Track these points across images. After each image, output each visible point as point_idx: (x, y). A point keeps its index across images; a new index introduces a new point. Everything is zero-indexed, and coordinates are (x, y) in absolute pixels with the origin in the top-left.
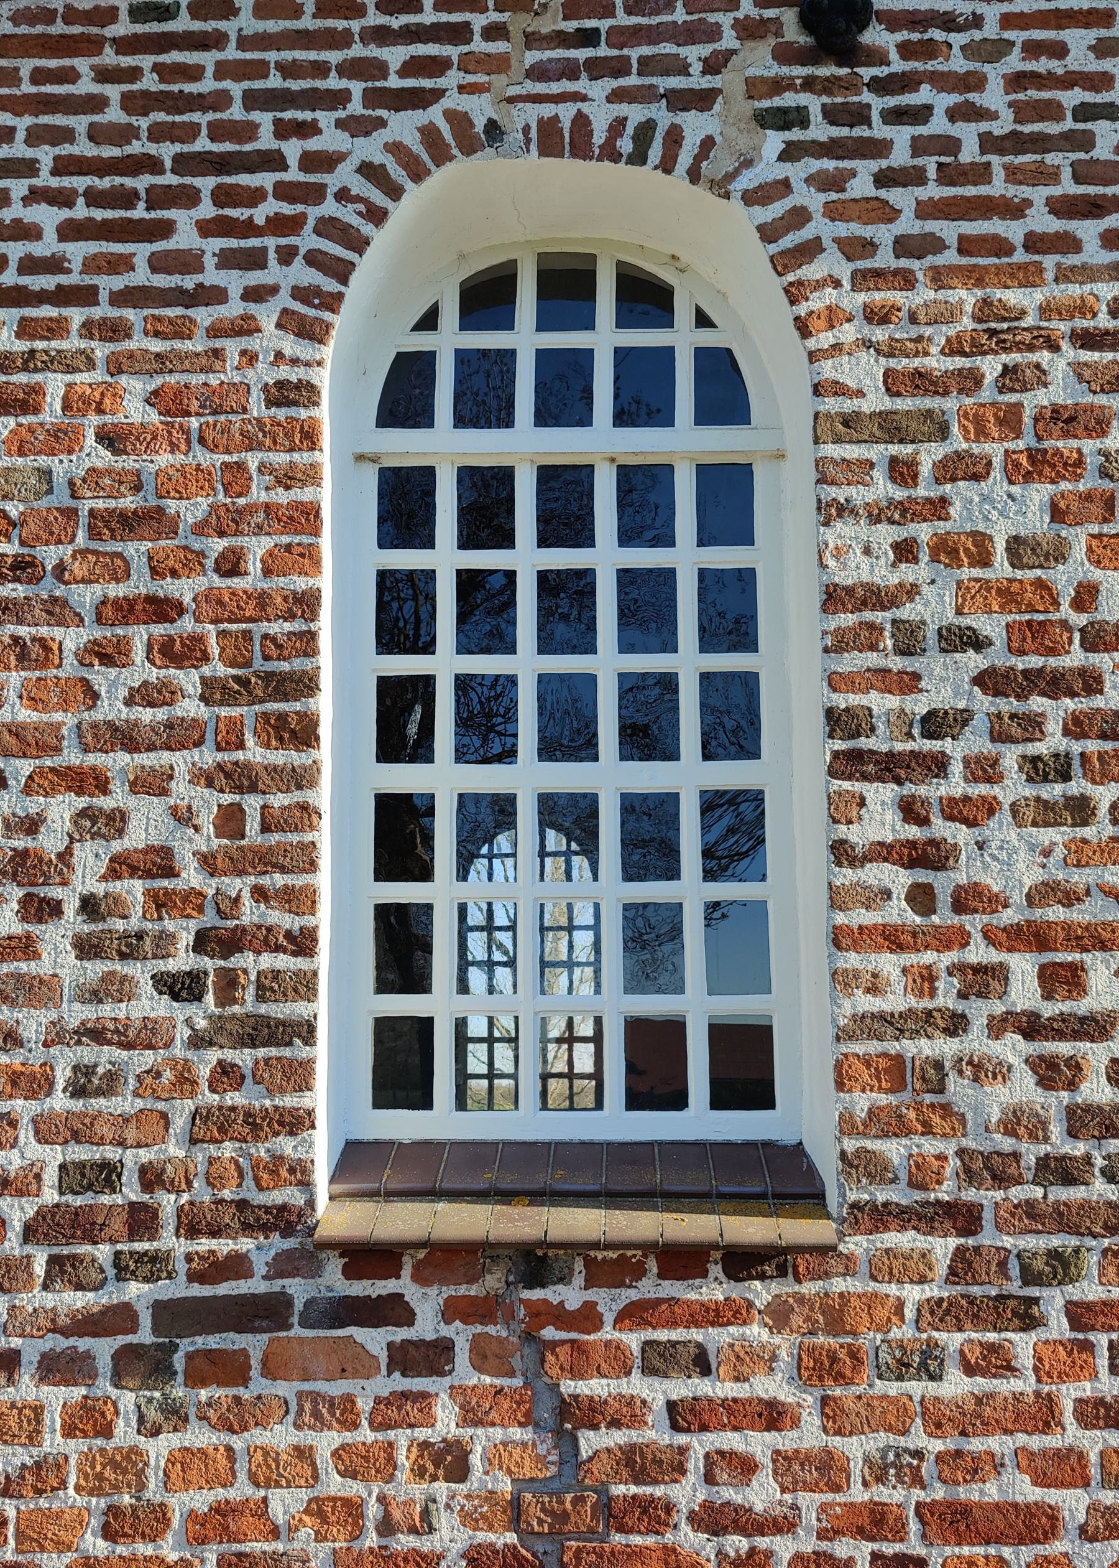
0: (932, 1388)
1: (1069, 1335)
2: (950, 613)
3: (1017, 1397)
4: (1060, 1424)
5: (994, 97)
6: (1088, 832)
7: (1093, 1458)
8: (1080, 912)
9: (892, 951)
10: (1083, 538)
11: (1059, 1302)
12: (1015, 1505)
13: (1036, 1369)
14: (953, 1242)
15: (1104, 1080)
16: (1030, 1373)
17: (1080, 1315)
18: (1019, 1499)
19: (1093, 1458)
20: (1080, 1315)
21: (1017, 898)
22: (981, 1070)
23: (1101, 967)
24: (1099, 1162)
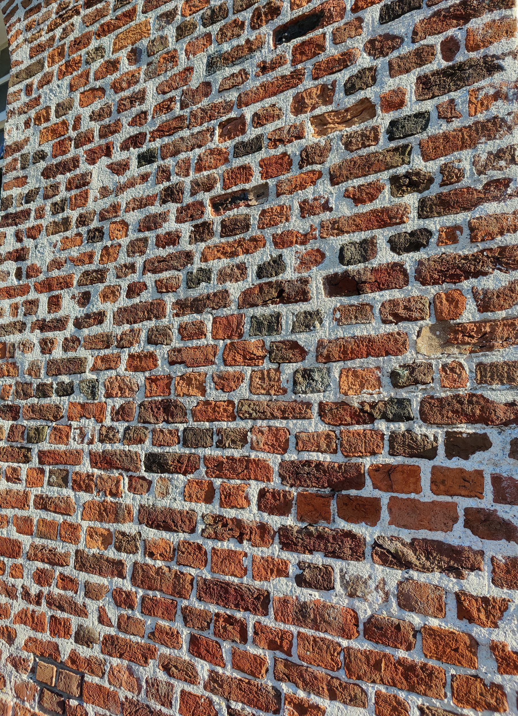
0: (37, 608)
1: (37, 465)
2: (37, 145)
3: (18, 492)
4: (28, 506)
5: (171, 321)
6: (68, 234)
7: (35, 522)
8: (63, 271)
9: (8, 298)
10: (79, 95)
11: (36, 451)
12: (10, 540)
13: (26, 481)
14: (11, 422)
15: (61, 348)
16: (24, 482)
17: (42, 455)
18: (11, 537)
19: (35, 522)
20: (42, 455)
21: (44, 269)
22: (25, 346)
23: (66, 295)
24: (55, 386)
